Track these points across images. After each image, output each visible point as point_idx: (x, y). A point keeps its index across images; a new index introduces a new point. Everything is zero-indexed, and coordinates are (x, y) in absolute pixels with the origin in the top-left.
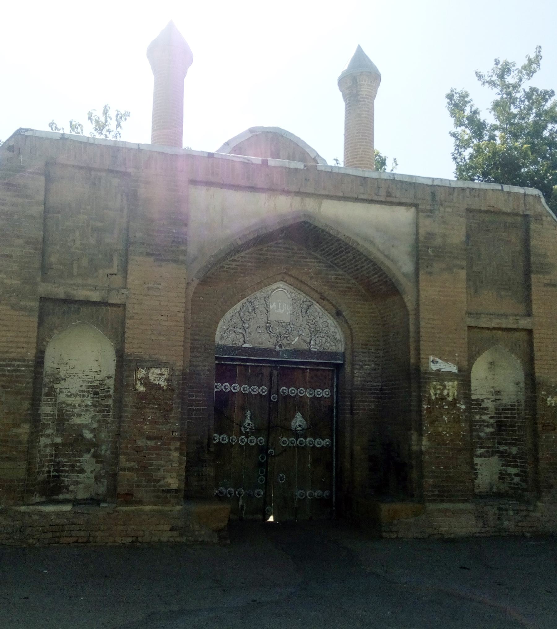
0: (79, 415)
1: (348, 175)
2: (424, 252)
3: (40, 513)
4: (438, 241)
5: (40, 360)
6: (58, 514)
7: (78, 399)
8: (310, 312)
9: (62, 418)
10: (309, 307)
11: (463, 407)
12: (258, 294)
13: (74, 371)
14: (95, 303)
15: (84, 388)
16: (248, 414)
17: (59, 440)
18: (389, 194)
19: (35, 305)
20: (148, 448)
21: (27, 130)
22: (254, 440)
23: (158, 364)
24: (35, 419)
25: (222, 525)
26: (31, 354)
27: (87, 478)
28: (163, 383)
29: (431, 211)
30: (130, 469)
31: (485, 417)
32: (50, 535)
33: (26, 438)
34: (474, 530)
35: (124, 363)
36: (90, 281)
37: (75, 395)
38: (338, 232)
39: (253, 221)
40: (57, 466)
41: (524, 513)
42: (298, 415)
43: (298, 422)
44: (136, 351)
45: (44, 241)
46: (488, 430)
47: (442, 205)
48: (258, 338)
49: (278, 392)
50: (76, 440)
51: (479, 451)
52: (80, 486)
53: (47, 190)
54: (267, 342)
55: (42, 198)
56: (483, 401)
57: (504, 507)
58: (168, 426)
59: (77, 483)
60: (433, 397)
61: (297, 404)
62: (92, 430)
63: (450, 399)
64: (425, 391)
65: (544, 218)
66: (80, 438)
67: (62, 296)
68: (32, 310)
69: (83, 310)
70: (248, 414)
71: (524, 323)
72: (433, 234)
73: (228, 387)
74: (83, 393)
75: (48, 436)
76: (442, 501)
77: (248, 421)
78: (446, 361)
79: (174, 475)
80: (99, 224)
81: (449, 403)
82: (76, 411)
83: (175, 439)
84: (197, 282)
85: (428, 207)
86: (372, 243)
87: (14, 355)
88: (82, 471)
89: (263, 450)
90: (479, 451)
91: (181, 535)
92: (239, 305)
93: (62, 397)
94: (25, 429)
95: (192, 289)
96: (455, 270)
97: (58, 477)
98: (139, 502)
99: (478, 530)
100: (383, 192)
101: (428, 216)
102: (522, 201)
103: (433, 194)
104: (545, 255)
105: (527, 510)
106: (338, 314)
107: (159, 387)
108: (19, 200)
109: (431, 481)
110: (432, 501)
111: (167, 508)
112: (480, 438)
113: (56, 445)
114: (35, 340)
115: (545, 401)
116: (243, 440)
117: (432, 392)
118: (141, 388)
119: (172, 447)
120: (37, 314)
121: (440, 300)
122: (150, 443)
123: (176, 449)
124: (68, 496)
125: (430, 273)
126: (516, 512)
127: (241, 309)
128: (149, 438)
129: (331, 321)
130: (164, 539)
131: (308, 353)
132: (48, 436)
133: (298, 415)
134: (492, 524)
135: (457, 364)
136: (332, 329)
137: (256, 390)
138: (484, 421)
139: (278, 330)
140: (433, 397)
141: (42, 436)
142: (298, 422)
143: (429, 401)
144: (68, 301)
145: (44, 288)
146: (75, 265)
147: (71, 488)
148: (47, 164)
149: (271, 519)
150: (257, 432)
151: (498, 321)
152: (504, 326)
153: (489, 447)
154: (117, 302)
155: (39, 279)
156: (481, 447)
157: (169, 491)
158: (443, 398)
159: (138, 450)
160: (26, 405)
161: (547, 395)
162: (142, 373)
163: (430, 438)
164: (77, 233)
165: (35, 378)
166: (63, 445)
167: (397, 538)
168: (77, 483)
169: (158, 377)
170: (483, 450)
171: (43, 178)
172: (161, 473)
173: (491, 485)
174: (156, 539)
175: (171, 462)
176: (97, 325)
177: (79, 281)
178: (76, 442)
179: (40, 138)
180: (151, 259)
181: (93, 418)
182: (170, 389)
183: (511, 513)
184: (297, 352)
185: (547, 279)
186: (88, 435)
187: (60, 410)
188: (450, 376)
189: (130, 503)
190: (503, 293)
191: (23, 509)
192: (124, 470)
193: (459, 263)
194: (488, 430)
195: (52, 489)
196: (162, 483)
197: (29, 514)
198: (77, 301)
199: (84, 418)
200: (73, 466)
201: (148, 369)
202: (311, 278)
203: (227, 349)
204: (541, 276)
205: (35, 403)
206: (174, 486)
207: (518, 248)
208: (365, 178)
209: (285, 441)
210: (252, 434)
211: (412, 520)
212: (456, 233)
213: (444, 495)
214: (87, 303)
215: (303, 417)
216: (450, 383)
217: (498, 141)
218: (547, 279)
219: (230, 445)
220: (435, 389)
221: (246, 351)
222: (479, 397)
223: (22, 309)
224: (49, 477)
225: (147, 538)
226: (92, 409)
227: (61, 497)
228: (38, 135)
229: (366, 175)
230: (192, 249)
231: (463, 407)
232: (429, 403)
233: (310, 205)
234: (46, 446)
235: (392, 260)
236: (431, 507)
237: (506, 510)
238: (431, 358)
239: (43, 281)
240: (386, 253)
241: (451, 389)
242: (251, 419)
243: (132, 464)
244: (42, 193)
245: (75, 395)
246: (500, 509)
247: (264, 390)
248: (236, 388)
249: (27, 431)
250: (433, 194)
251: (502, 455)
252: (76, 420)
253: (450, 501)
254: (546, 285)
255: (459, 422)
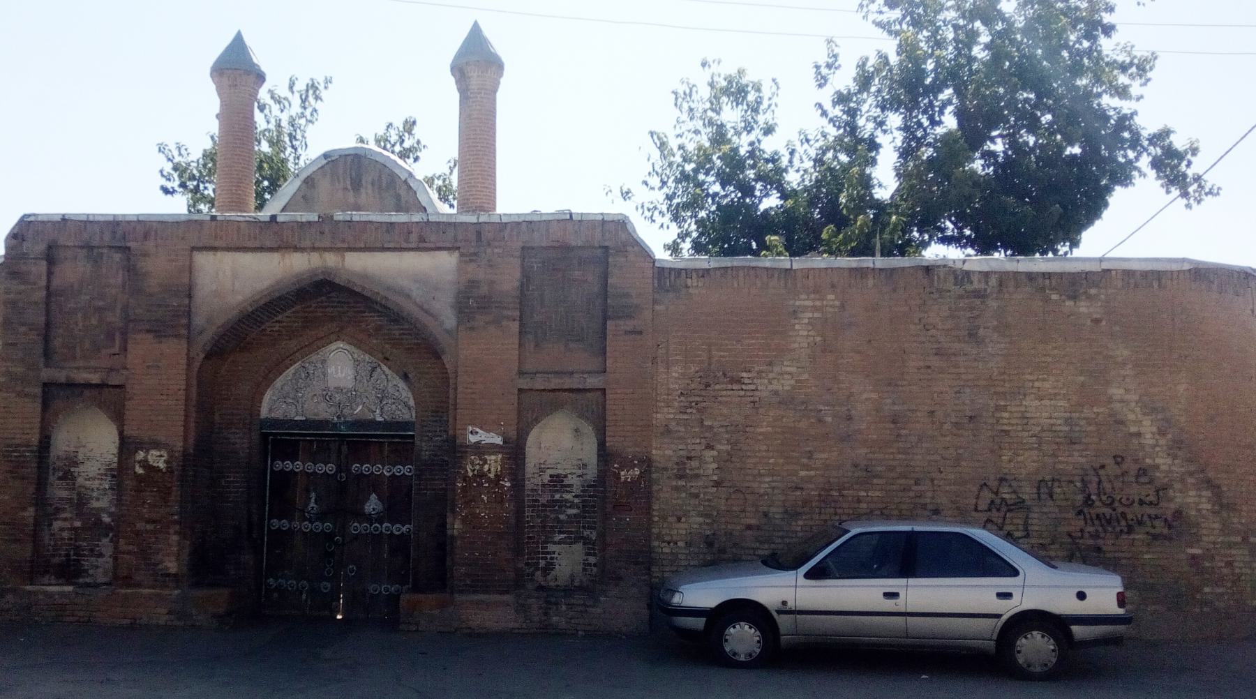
0: (98, 499)
1: (370, 222)
2: (473, 303)
3: (46, 593)
4: (484, 290)
5: (45, 444)
6: (62, 594)
7: (97, 482)
8: (375, 375)
9: (80, 504)
10: (374, 369)
11: (508, 484)
12: (314, 357)
13: (92, 454)
14: (97, 386)
15: (102, 471)
16: (313, 495)
17: (78, 524)
18: (422, 239)
19: (38, 391)
20: (147, 532)
21: (29, 216)
22: (319, 526)
23: (156, 445)
24: (41, 499)
25: (221, 611)
26: (35, 439)
27: (106, 562)
28: (162, 465)
29: (475, 254)
30: (129, 553)
31: (568, 496)
32: (53, 614)
33: (31, 520)
34: (511, 625)
35: (127, 446)
36: (93, 363)
37: (94, 479)
38: (364, 288)
39: (266, 283)
40: (77, 549)
41: (580, 609)
42: (373, 496)
43: (373, 504)
44: (135, 433)
45: (48, 325)
46: (571, 511)
47: (489, 245)
48: (313, 407)
49: (348, 471)
50: (95, 524)
51: (558, 537)
52: (101, 570)
53: (50, 274)
54: (323, 411)
55: (43, 283)
56: (566, 476)
57: (553, 600)
58: (168, 510)
59: (97, 567)
60: (470, 474)
61: (374, 483)
62: (111, 514)
63: (492, 475)
64: (460, 467)
65: (629, 249)
66: (99, 522)
67: (63, 380)
68: (35, 396)
69: (87, 393)
70: (313, 495)
71: (593, 381)
72: (477, 282)
73: (289, 465)
74: (101, 477)
75: (65, 519)
76: (474, 592)
77: (312, 505)
78: (488, 431)
79: (173, 559)
80: (101, 303)
81: (489, 481)
82: (95, 494)
83: (175, 522)
84: (202, 356)
85: (472, 250)
86: (408, 296)
87: (18, 442)
88: (101, 555)
89: (329, 537)
90: (558, 537)
91: (179, 619)
92: (292, 369)
93: (80, 480)
94: (31, 512)
95: (197, 364)
96: (504, 323)
97: (78, 561)
98: (139, 585)
99: (517, 625)
100: (414, 237)
101: (471, 261)
102: (598, 230)
103: (479, 234)
104: (627, 295)
105: (584, 605)
106: (405, 377)
107: (158, 470)
108: (23, 287)
109: (463, 570)
110: (461, 592)
111: (167, 592)
112: (559, 521)
113: (75, 529)
114: (38, 425)
115: (618, 476)
116: (307, 526)
117: (469, 467)
118: (140, 471)
119: (171, 531)
120: (40, 400)
121: (488, 358)
122: (150, 527)
123: (176, 533)
124: (88, 580)
125: (472, 329)
126: (570, 606)
127: (294, 374)
128: (148, 521)
129: (402, 385)
130: (161, 622)
131: (373, 424)
132: (65, 519)
133: (373, 496)
134: (536, 619)
135: (503, 434)
136: (404, 394)
137: (322, 468)
138: (566, 501)
139: (338, 397)
140: (470, 474)
141: (56, 519)
142: (373, 504)
143: (465, 478)
144: (71, 385)
145: (47, 374)
146: (78, 349)
147: (91, 572)
148: (50, 247)
149: (339, 617)
150: (322, 517)
151: (558, 381)
152: (566, 387)
153: (571, 532)
154: (116, 383)
155: (41, 365)
156: (560, 533)
157: (168, 575)
158: (482, 475)
159: (138, 533)
160: (32, 489)
161: (621, 468)
162: (141, 455)
163: (464, 520)
164: (80, 315)
165: (39, 463)
166: (82, 528)
167: (417, 631)
168: (97, 567)
169: (158, 459)
170: (563, 536)
171: (44, 263)
172: (160, 557)
173: (572, 578)
174: (154, 622)
175: (170, 546)
176: (100, 408)
177: (81, 363)
178: (95, 526)
179: (43, 222)
180: (150, 336)
181: (111, 502)
182: (170, 470)
183: (564, 608)
184: (359, 424)
185: (629, 325)
186: (106, 519)
187: (79, 494)
188: (493, 448)
189: (129, 586)
190: (572, 345)
191: (29, 588)
192: (123, 553)
193: (509, 313)
194: (571, 511)
195: (69, 571)
196: (160, 567)
197: (36, 593)
198: (80, 385)
199: (102, 502)
200: (92, 550)
201: (147, 451)
202: (370, 336)
203: (275, 423)
204: (621, 322)
205: (41, 484)
206: (173, 570)
207: (596, 290)
208: (391, 223)
209: (356, 527)
210: (318, 519)
211: (436, 612)
212: (508, 278)
213: (480, 584)
214: (88, 386)
215: (379, 499)
216: (493, 457)
217: (979, 52)
218: (629, 325)
219: (291, 532)
220: (472, 463)
221: (297, 424)
222: (561, 472)
223: (26, 395)
224: (68, 560)
225: (145, 620)
226: (110, 492)
227: (81, 580)
228: (40, 219)
229: (394, 219)
230: (199, 321)
231: (508, 484)
232: (465, 480)
233: (331, 260)
234: (62, 529)
235: (431, 315)
236: (458, 597)
237: (556, 604)
238: (470, 428)
239: (47, 366)
240: (426, 307)
241: (493, 464)
242: (316, 502)
243: (131, 547)
244: (44, 278)
245: (94, 479)
246: (547, 602)
247: (330, 468)
248: (298, 466)
249: (33, 514)
250: (479, 234)
251: (586, 541)
252: (95, 504)
253: (487, 592)
254: (627, 332)
255: (502, 501)
